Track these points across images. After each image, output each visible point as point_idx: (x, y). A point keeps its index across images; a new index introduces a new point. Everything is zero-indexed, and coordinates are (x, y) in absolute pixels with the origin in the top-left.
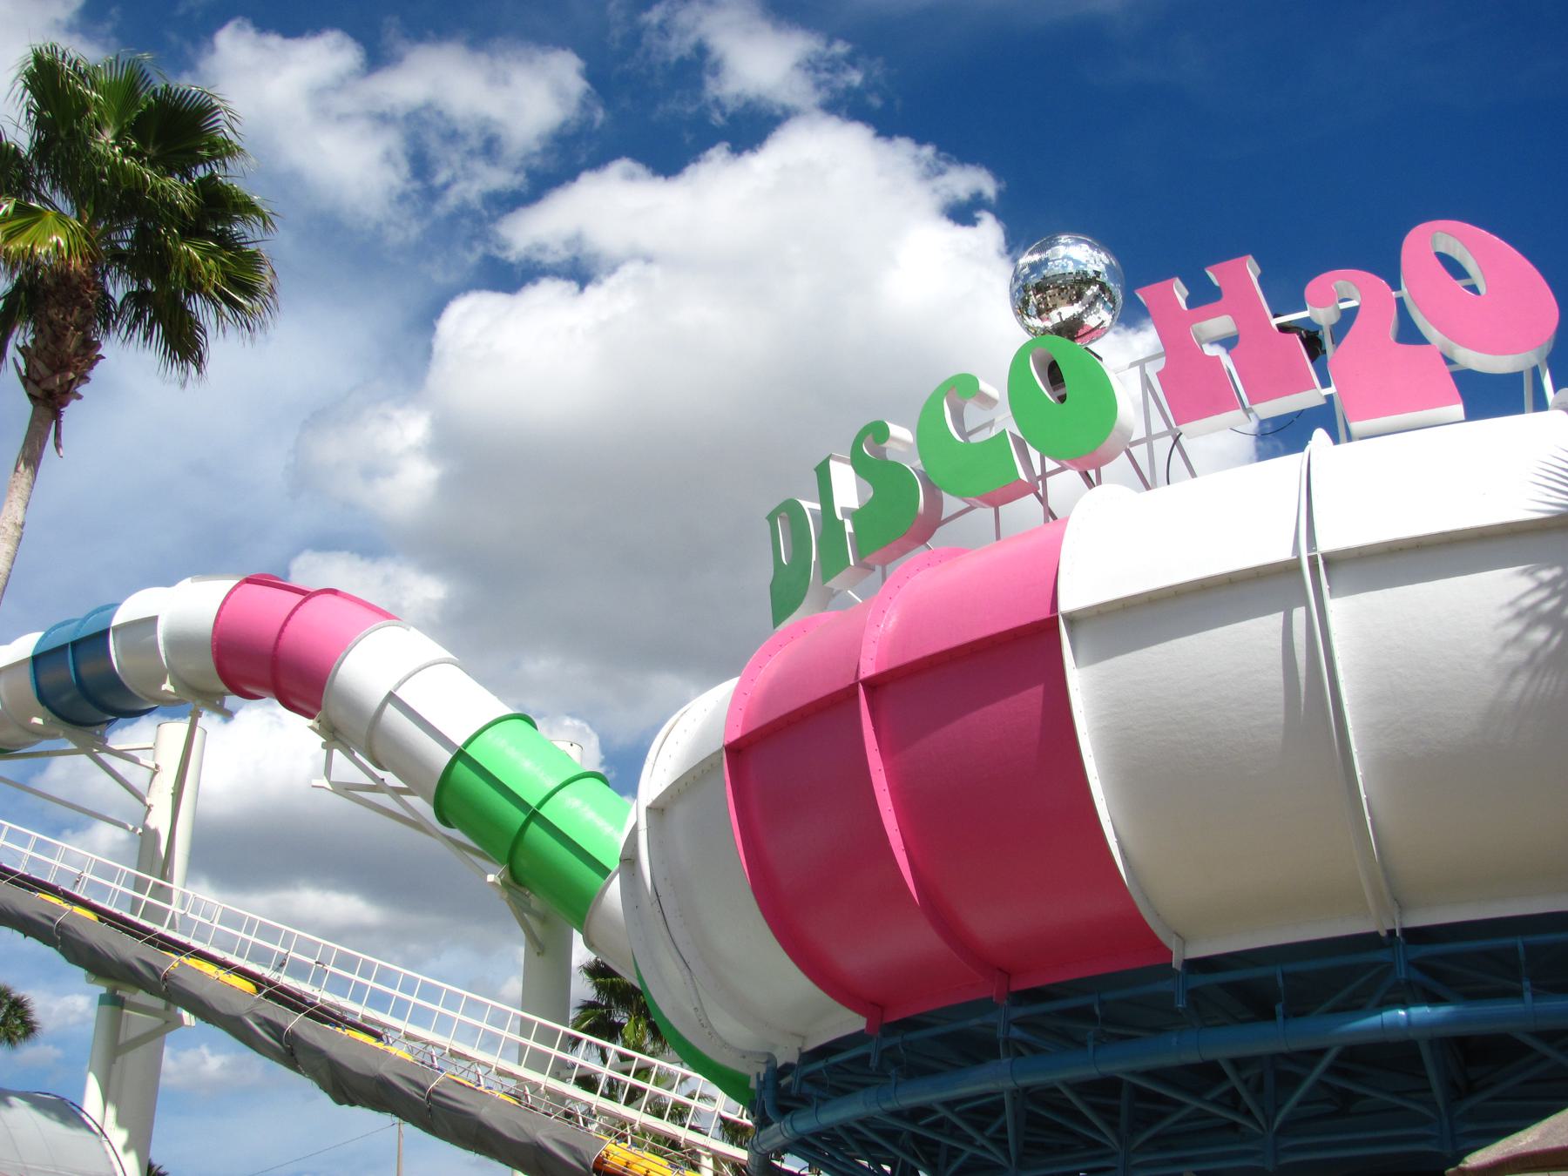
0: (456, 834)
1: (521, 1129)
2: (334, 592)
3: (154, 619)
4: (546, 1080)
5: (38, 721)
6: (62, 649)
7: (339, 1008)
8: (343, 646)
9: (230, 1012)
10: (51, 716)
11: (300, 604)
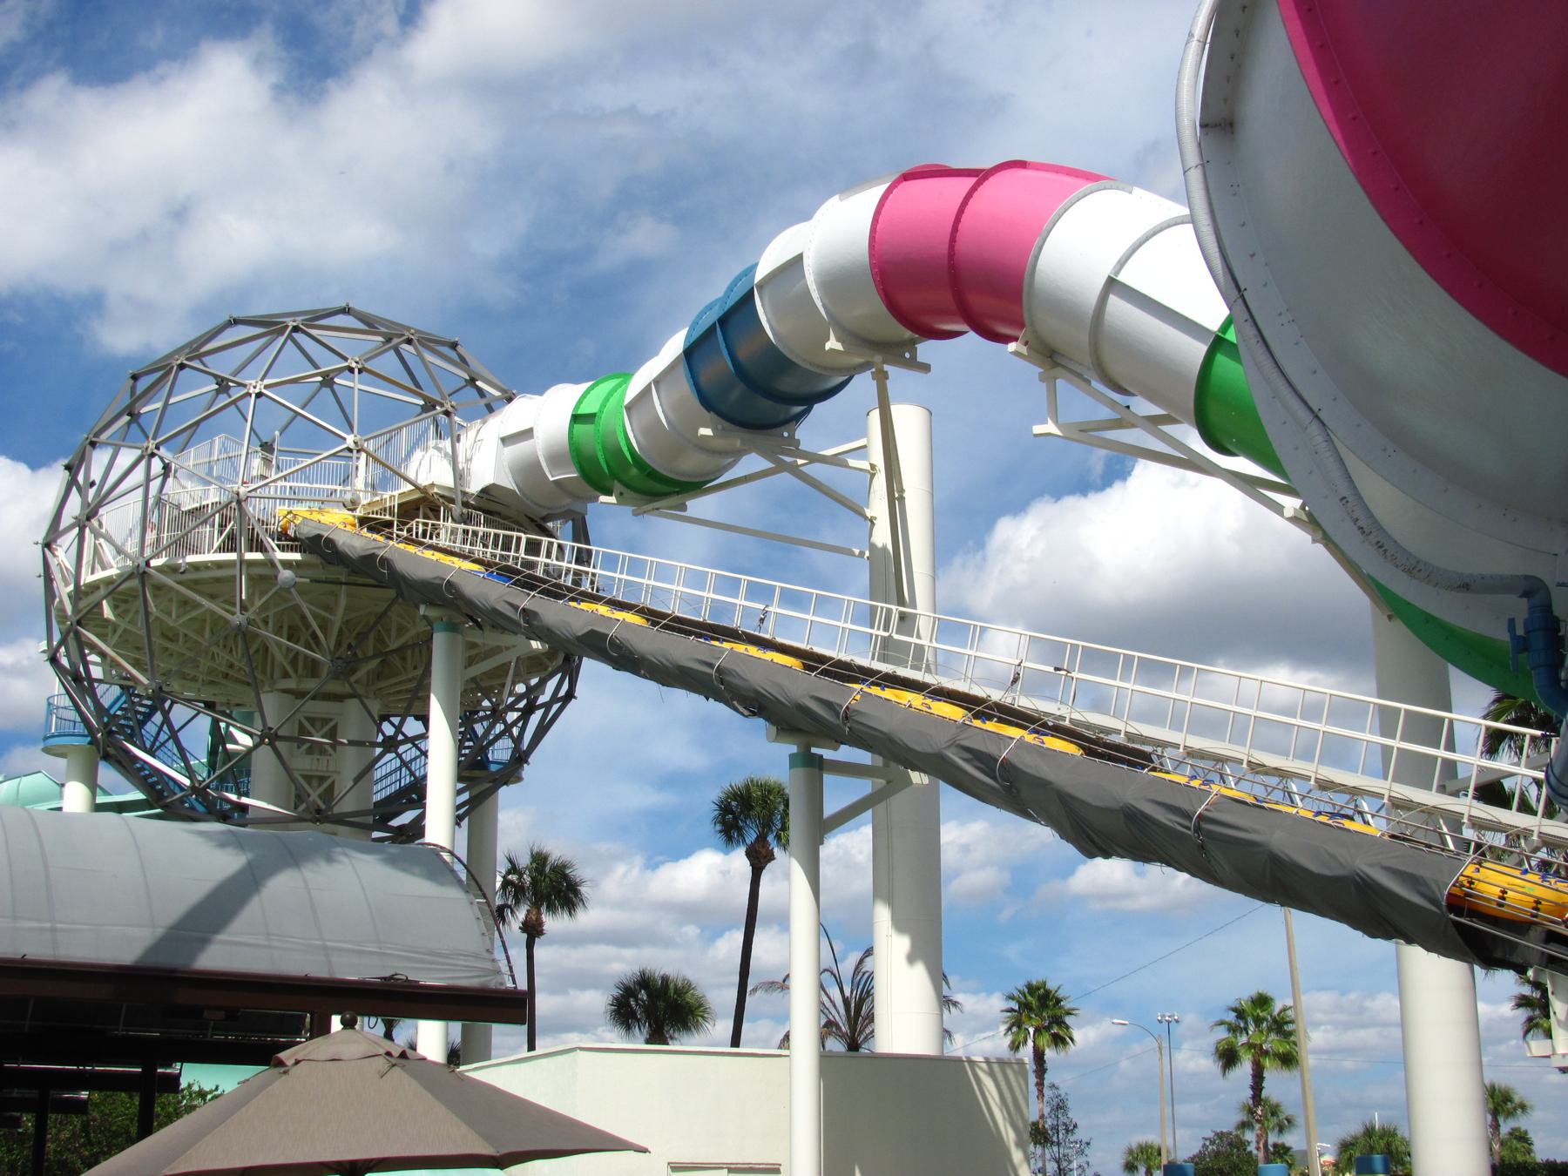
0: (1242, 464)
1: (1333, 857)
2: (1021, 164)
3: (798, 260)
4: (1431, 798)
5: (705, 431)
6: (709, 333)
7: (1089, 726)
8: (1037, 233)
9: (929, 750)
10: (722, 423)
11: (974, 189)
